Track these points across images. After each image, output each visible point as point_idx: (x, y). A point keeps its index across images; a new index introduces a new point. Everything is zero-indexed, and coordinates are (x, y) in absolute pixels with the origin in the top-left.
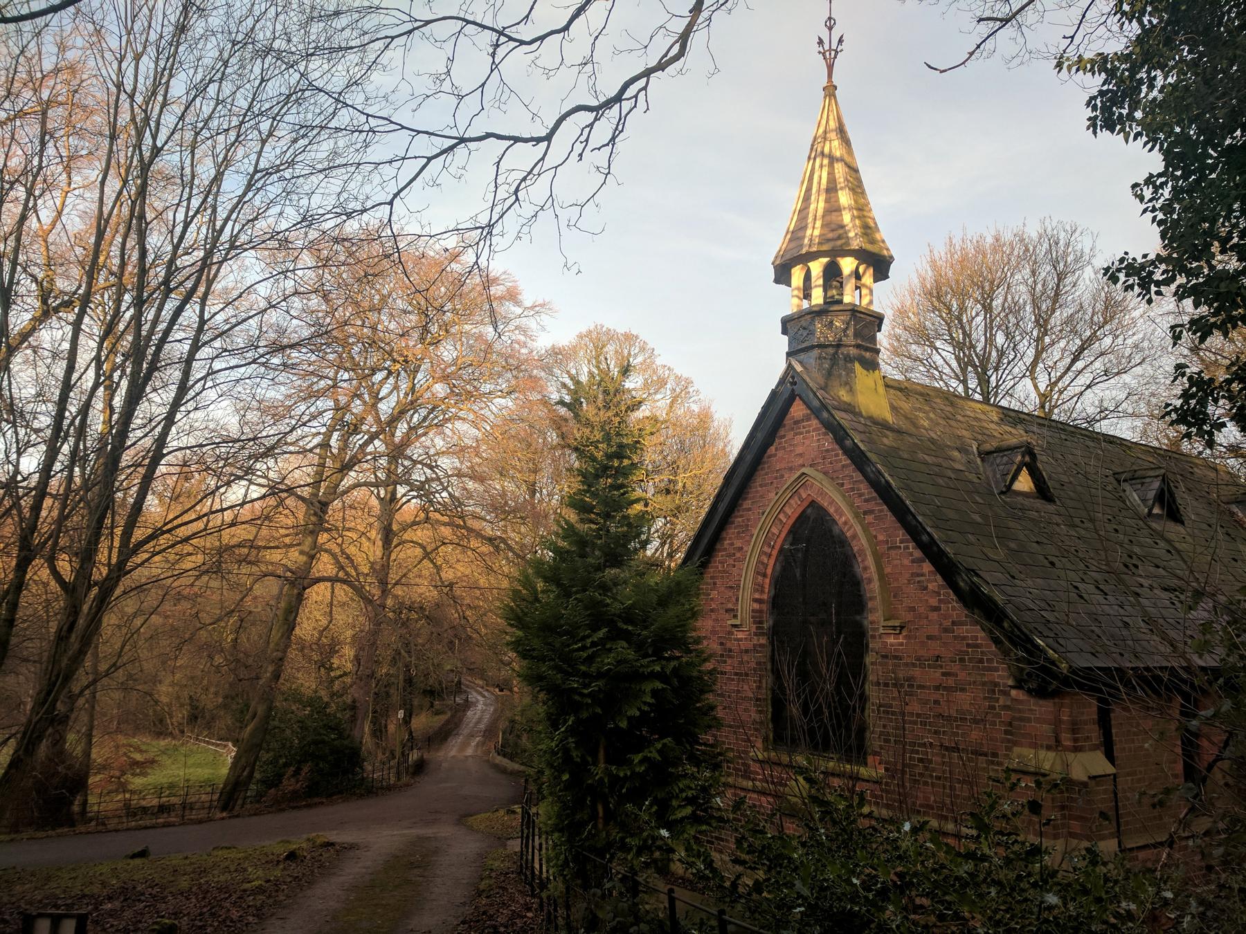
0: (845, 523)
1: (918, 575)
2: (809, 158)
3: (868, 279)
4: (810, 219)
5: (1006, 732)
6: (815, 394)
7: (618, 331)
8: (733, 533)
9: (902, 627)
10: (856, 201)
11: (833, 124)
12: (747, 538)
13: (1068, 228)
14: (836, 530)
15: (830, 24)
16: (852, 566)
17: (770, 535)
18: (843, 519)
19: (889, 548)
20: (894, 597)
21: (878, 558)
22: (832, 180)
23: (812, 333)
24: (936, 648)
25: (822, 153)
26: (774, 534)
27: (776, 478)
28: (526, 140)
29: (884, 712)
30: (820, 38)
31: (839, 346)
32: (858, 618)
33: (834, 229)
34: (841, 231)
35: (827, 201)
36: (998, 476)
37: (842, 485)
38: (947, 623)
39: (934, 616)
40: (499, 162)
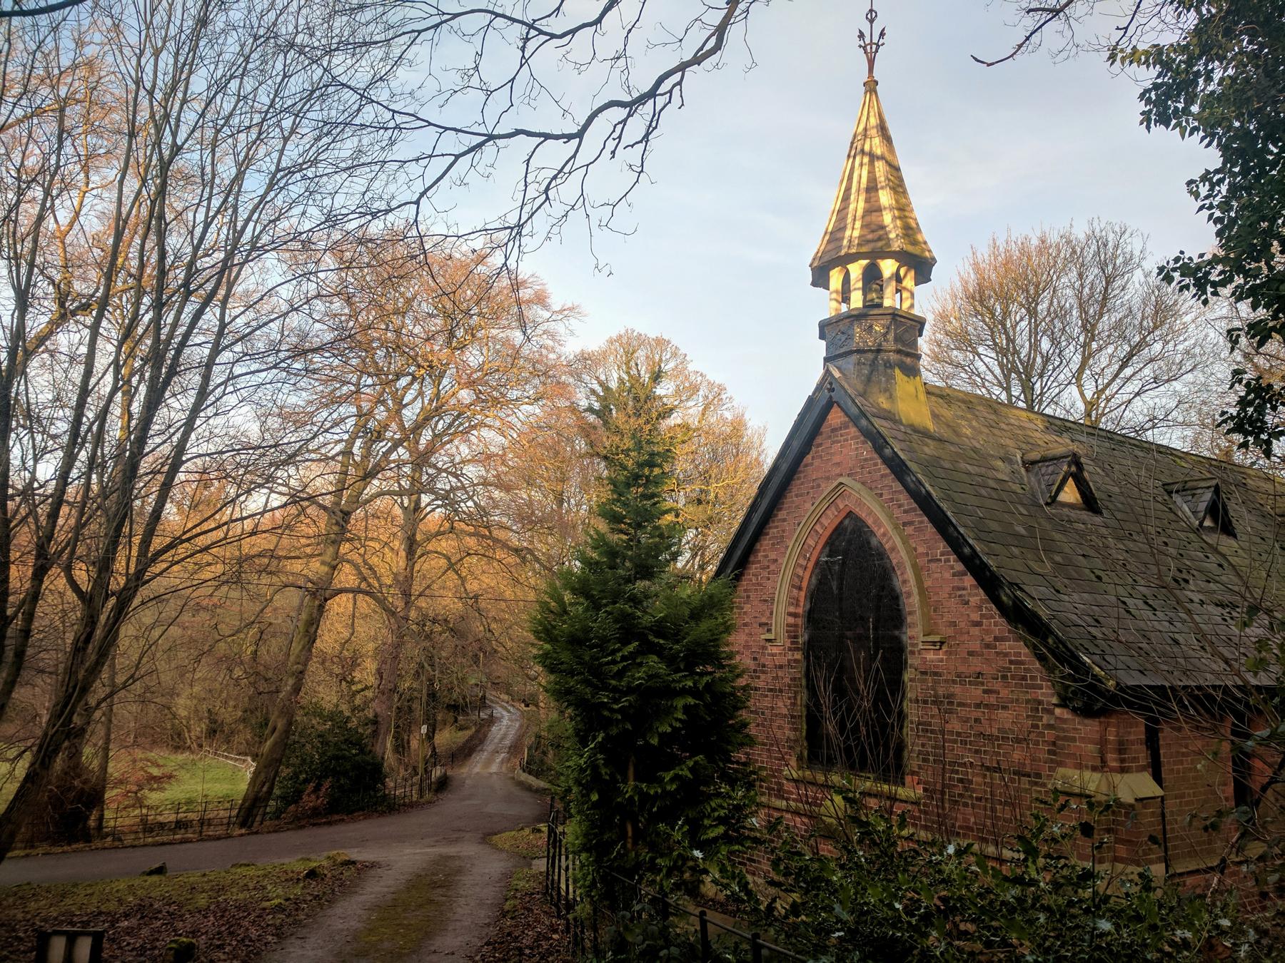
0: (884, 535)
1: (959, 589)
2: (849, 156)
4: (849, 220)
6: (853, 401)
9: (942, 643)
10: (897, 201)
13: (1117, 229)
14: (874, 542)
16: (890, 579)
19: (929, 561)
24: (976, 664)
25: (862, 151)
26: (809, 546)
28: (557, 137)
31: (879, 351)
32: (897, 633)
33: (874, 229)
34: (881, 232)
35: (867, 201)
38: (989, 639)
39: (975, 631)
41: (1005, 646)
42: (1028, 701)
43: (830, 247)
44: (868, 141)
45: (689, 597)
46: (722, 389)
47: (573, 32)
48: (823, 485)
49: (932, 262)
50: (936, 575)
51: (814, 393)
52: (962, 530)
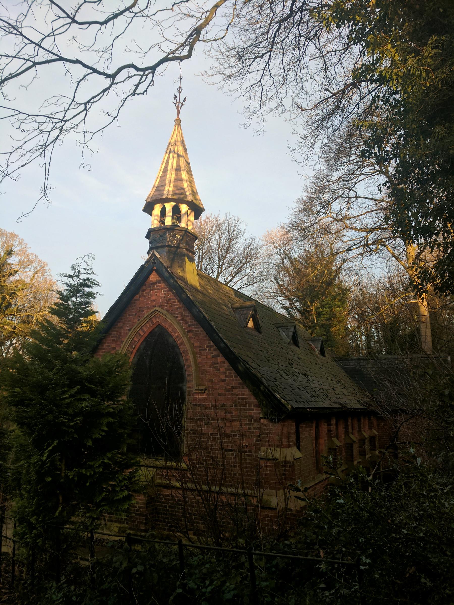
0: (177, 336)
1: (215, 364)
2: (166, 152)
3: (192, 218)
4: (167, 182)
5: (257, 440)
6: (167, 270)
7: (6, 230)
9: (206, 389)
10: (189, 178)
11: (179, 139)
13: (236, 219)
14: (171, 340)
15: (180, 90)
17: (133, 341)
19: (200, 350)
20: (202, 374)
21: (194, 354)
23: (166, 239)
25: (174, 151)
26: (135, 341)
27: (139, 311)
30: (175, 95)
32: (180, 385)
33: (179, 190)
34: (182, 191)
35: (176, 175)
36: (242, 319)
37: (177, 317)
38: (229, 387)
39: (223, 384)
40: (79, 82)
41: (237, 391)
42: (247, 417)
43: (157, 193)
45: (109, 361)
47: (90, 23)
48: (145, 311)
49: (202, 210)
50: (203, 357)
51: (145, 264)
52: (221, 335)
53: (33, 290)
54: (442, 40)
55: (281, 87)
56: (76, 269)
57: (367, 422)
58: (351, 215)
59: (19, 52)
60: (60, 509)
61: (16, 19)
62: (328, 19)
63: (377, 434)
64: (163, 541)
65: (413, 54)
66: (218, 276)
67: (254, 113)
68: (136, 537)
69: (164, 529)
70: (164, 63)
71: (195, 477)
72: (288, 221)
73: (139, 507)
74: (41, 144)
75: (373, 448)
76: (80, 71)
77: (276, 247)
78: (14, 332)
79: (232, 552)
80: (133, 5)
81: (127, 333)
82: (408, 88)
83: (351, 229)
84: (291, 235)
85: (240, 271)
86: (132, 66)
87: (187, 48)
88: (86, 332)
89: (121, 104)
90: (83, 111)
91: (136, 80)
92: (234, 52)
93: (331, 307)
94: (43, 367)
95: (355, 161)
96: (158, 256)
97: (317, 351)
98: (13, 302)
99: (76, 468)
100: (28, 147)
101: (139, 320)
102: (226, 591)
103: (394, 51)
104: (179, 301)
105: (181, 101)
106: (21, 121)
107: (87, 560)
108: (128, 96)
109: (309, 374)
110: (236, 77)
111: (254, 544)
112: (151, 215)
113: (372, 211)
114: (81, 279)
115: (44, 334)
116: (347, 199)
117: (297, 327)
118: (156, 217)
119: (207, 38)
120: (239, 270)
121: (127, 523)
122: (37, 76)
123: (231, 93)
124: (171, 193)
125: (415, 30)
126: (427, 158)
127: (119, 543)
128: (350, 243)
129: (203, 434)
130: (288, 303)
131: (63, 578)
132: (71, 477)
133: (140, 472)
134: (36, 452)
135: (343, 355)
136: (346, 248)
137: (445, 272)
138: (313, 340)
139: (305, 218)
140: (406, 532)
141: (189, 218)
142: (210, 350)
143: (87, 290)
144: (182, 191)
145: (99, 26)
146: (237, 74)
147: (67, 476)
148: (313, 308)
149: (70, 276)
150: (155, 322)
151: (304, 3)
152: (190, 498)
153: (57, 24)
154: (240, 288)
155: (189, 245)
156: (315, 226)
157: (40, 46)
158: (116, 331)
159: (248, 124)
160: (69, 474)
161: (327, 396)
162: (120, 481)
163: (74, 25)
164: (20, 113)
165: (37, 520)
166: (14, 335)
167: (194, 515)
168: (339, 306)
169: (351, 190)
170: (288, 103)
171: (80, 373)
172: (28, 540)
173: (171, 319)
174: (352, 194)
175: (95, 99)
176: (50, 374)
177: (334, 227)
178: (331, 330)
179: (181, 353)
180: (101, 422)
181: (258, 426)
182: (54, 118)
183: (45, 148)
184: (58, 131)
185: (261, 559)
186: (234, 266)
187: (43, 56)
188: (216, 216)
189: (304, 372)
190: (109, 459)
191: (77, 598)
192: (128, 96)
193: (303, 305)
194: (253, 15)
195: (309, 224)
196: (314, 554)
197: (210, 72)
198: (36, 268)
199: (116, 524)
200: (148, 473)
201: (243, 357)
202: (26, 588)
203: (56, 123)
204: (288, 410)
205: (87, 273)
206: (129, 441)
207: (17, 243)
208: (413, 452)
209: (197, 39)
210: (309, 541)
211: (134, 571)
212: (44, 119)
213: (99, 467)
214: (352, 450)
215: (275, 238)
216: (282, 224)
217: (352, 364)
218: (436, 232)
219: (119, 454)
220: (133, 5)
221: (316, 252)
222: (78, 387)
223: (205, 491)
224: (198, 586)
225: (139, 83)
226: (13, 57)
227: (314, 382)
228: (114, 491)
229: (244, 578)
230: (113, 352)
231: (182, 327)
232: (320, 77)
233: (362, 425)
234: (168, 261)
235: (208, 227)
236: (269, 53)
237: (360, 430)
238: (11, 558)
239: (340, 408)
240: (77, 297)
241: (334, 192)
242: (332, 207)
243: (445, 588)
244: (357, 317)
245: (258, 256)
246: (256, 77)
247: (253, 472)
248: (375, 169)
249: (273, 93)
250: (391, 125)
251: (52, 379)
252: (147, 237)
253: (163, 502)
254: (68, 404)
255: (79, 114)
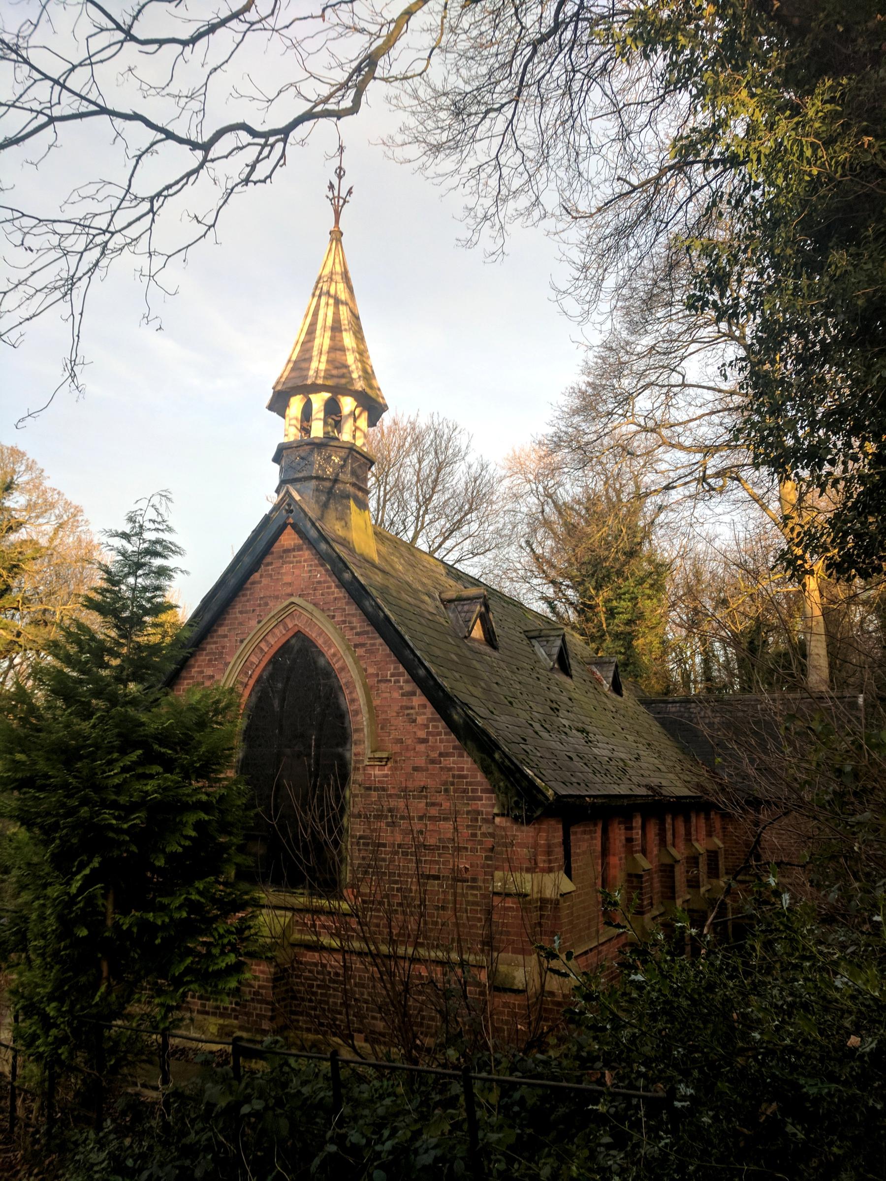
0: (334, 655)
1: (408, 708)
2: (314, 295)
3: (363, 422)
4: (315, 353)
5: (487, 858)
6: (313, 524)
8: (204, 661)
9: (388, 759)
11: (338, 268)
12: (221, 666)
13: (450, 425)
14: (322, 662)
15: (340, 173)
16: (336, 698)
17: (248, 663)
18: (332, 651)
19: (379, 682)
20: (382, 728)
21: (368, 689)
22: (337, 321)
23: (311, 464)
24: (421, 779)
25: (328, 293)
26: (252, 663)
27: (260, 605)
28: (181, 141)
29: (364, 844)
31: (336, 481)
32: (340, 750)
33: (338, 366)
34: (344, 371)
35: (332, 338)
37: (333, 617)
38: (434, 755)
39: (421, 748)
40: (140, 157)
41: (450, 762)
42: (468, 813)
43: (293, 374)
44: (333, 284)
45: (199, 702)
46: (78, 510)
47: (161, 42)
48: (271, 604)
49: (384, 408)
50: (385, 695)
51: (272, 512)
52: (418, 653)
53: (55, 560)
54: (841, 85)
55: (538, 169)
56: (135, 522)
57: (702, 822)
58: (672, 421)
59: (21, 96)
60: (103, 989)
61: (16, 32)
62: (624, 41)
63: (721, 846)
64: (305, 1054)
65: (788, 113)
66: (415, 537)
67: (485, 218)
68: (251, 1045)
69: (308, 1030)
70: (306, 123)
71: (365, 928)
72: (551, 431)
73: (260, 987)
74: (64, 275)
75: (713, 872)
76: (141, 135)
77: (530, 481)
78: (16, 642)
79: (433, 1076)
80: (246, 9)
81: (237, 647)
82: (777, 177)
83: (673, 446)
84: (558, 457)
85: (459, 528)
86: (244, 127)
87: (352, 93)
88: (156, 645)
89: (222, 201)
90: (147, 213)
91: (252, 153)
92: (445, 101)
93: (634, 599)
94: (71, 714)
95: (680, 315)
96: (297, 497)
97: (606, 686)
98: (14, 584)
99: (137, 911)
100: (38, 281)
101: (259, 622)
102: (421, 1151)
103: (752, 103)
104: (337, 586)
105: (343, 194)
106: (26, 230)
107: (156, 1088)
108: (237, 185)
109: (589, 728)
110: (449, 148)
111: (479, 1059)
112: (284, 417)
113: (713, 413)
114: (144, 542)
115: (73, 649)
116: (665, 390)
117: (567, 638)
118: (294, 422)
119: (393, 73)
120: (457, 526)
121: (236, 1018)
122: (58, 143)
123: (441, 179)
124: (322, 374)
125: (790, 67)
126: (814, 313)
127: (221, 1056)
128: (672, 474)
129: (384, 845)
130: (552, 590)
131: (108, 1124)
132: (125, 927)
133: (261, 918)
134: (57, 877)
135: (658, 693)
136: (665, 484)
137: (846, 534)
138: (600, 663)
139: (584, 426)
140: (758, 1037)
141: (359, 423)
142: (398, 681)
143: (157, 562)
144: (344, 371)
145: (179, 47)
146: (452, 143)
147: (117, 926)
148: (600, 600)
149: (125, 536)
150: (290, 626)
151: (581, 6)
152: (358, 970)
153: (98, 43)
154: (458, 561)
155: (357, 477)
156: (606, 440)
157: (63, 86)
158: (216, 643)
159: (474, 239)
160: (121, 922)
161: (624, 771)
162: (221, 936)
163: (130, 46)
164: (24, 215)
165: (58, 1010)
166: (17, 648)
167: (366, 1002)
168: (649, 597)
169: (673, 370)
170: (551, 200)
171: (143, 724)
172: (41, 1049)
173: (322, 620)
174: (676, 379)
175: (171, 191)
176: (85, 726)
177: (641, 443)
178: (635, 643)
179: (341, 687)
180: (184, 820)
181: (491, 830)
182: (89, 227)
183: (73, 284)
184: (97, 252)
185: (490, 1090)
186: (447, 516)
187: (68, 104)
188: (412, 420)
189: (580, 725)
190: (200, 893)
191: (135, 1161)
192: (237, 185)
193: (583, 595)
194: (483, 29)
195: (594, 437)
196: (593, 1079)
197: (399, 138)
198: (59, 517)
199: (212, 1019)
200: (276, 921)
201: (461, 696)
202: (37, 1141)
203: (94, 236)
204: (547, 798)
205: (157, 530)
206: (239, 859)
207: (23, 468)
208: (773, 884)
209: (371, 76)
210: (584, 1054)
211: (245, 1109)
212: (68, 228)
213: (179, 908)
214: (673, 878)
215: (527, 463)
216: (540, 438)
217: (674, 709)
218: (829, 457)
219: (220, 883)
220: (246, 9)
221: (607, 491)
222: (139, 752)
223: (385, 956)
224: (369, 1140)
225: (258, 161)
226: (9, 106)
227: (599, 745)
228: (209, 956)
229: (456, 1126)
230: (207, 683)
231: (343, 638)
232: (612, 151)
233: (693, 829)
234: (316, 507)
235: (396, 440)
236: (514, 103)
237: (688, 840)
238: (9, 1083)
239: (648, 796)
240: (137, 577)
241: (642, 375)
242: (637, 405)
243: (831, 1144)
244: (685, 618)
245: (494, 498)
246: (489, 148)
247: (480, 920)
248: (719, 332)
249: (522, 181)
250: (747, 247)
251: (87, 738)
252: (277, 459)
253: (306, 978)
254: (118, 786)
255: (139, 219)
